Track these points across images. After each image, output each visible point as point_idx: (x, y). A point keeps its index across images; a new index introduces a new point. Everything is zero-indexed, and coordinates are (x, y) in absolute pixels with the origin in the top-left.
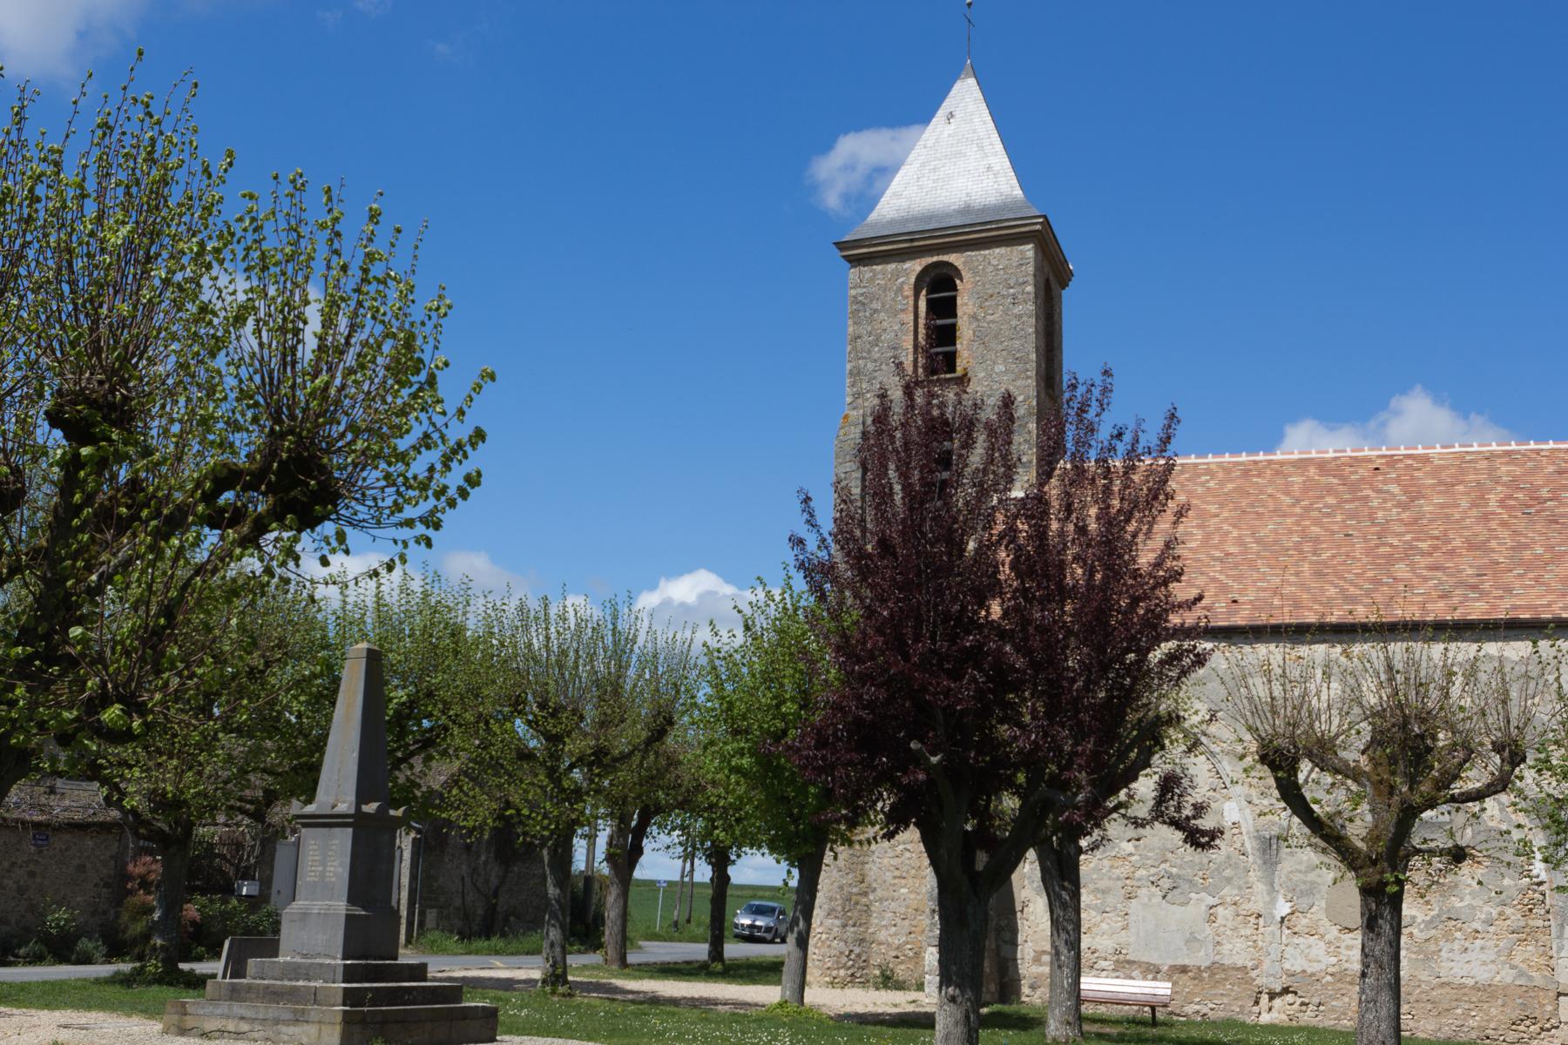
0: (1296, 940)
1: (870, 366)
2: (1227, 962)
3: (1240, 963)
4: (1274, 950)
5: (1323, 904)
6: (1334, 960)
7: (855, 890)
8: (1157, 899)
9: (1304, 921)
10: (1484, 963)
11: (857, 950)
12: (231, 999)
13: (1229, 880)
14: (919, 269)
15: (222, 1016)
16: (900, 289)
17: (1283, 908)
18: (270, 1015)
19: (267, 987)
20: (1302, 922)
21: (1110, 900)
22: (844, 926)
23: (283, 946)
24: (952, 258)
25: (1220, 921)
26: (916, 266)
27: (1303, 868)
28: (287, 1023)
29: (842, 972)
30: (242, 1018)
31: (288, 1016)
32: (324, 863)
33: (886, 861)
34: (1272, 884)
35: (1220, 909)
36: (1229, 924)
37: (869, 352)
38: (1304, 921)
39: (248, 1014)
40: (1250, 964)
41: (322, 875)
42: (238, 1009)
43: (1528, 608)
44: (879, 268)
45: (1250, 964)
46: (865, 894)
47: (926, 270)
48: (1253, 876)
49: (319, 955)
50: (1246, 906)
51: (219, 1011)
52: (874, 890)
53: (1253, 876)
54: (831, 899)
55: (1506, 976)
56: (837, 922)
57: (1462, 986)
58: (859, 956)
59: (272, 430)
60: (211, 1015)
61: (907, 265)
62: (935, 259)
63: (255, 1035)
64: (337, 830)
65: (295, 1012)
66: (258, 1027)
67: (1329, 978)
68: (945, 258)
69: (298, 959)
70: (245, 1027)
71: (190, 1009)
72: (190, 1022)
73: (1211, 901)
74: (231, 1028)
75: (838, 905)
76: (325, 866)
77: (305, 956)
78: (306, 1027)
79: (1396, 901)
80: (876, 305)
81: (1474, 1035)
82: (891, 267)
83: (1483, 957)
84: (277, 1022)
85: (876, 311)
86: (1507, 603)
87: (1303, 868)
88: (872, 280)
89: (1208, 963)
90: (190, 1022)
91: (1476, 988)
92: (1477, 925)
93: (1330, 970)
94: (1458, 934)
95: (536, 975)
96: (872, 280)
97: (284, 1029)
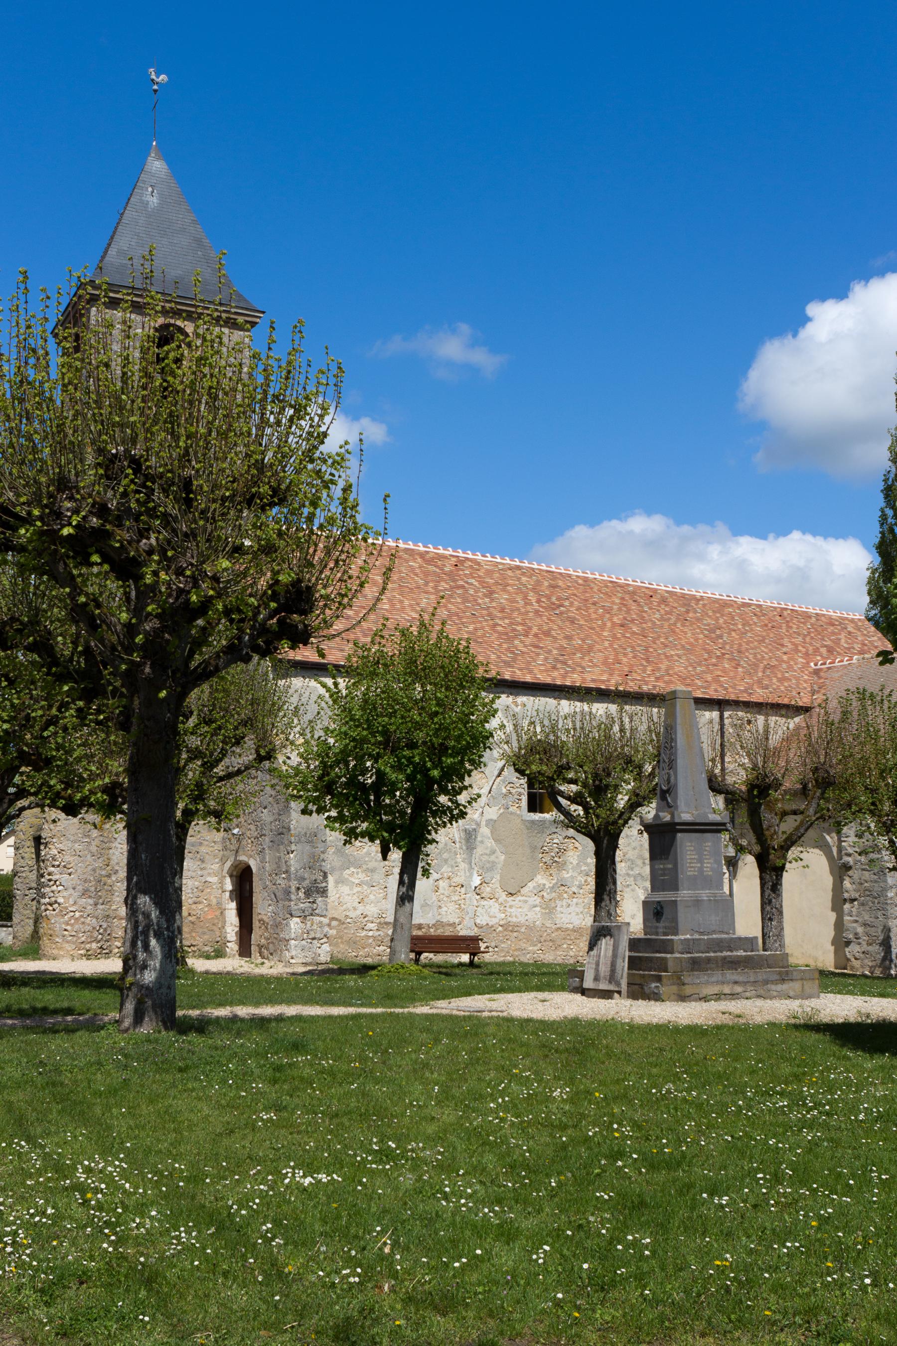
0: (483, 902)
2: (444, 920)
3: (451, 921)
4: (471, 910)
5: (498, 877)
6: (503, 916)
7: (103, 873)
9: (488, 889)
10: (577, 914)
11: (105, 925)
12: (692, 970)
13: (446, 861)
15: (717, 982)
17: (476, 881)
18: (760, 978)
19: (725, 958)
20: (486, 890)
21: (376, 877)
22: (96, 905)
23: (681, 926)
25: (441, 891)
27: (488, 852)
28: (772, 982)
29: (94, 945)
30: (736, 983)
31: (776, 977)
32: (701, 861)
34: (470, 863)
35: (441, 882)
36: (446, 893)
38: (488, 889)
39: (740, 978)
40: (457, 921)
41: (701, 870)
42: (731, 975)
43: (593, 681)
45: (457, 921)
46: (109, 876)
48: (459, 858)
49: (714, 932)
50: (455, 880)
51: (714, 979)
53: (459, 858)
54: (85, 881)
56: (91, 901)
57: (567, 929)
58: (105, 930)
60: (708, 983)
63: (748, 994)
64: (708, 835)
65: (780, 973)
66: (749, 988)
67: (500, 928)
69: (697, 936)
70: (738, 989)
72: (688, 990)
74: (727, 990)
75: (91, 886)
76: (702, 863)
77: (702, 933)
78: (791, 984)
79: (780, 870)
81: (572, 961)
83: (578, 910)
84: (766, 982)
86: (588, 677)
87: (488, 852)
89: (434, 922)
90: (688, 990)
92: (574, 889)
93: (502, 923)
94: (565, 895)
97: (773, 987)
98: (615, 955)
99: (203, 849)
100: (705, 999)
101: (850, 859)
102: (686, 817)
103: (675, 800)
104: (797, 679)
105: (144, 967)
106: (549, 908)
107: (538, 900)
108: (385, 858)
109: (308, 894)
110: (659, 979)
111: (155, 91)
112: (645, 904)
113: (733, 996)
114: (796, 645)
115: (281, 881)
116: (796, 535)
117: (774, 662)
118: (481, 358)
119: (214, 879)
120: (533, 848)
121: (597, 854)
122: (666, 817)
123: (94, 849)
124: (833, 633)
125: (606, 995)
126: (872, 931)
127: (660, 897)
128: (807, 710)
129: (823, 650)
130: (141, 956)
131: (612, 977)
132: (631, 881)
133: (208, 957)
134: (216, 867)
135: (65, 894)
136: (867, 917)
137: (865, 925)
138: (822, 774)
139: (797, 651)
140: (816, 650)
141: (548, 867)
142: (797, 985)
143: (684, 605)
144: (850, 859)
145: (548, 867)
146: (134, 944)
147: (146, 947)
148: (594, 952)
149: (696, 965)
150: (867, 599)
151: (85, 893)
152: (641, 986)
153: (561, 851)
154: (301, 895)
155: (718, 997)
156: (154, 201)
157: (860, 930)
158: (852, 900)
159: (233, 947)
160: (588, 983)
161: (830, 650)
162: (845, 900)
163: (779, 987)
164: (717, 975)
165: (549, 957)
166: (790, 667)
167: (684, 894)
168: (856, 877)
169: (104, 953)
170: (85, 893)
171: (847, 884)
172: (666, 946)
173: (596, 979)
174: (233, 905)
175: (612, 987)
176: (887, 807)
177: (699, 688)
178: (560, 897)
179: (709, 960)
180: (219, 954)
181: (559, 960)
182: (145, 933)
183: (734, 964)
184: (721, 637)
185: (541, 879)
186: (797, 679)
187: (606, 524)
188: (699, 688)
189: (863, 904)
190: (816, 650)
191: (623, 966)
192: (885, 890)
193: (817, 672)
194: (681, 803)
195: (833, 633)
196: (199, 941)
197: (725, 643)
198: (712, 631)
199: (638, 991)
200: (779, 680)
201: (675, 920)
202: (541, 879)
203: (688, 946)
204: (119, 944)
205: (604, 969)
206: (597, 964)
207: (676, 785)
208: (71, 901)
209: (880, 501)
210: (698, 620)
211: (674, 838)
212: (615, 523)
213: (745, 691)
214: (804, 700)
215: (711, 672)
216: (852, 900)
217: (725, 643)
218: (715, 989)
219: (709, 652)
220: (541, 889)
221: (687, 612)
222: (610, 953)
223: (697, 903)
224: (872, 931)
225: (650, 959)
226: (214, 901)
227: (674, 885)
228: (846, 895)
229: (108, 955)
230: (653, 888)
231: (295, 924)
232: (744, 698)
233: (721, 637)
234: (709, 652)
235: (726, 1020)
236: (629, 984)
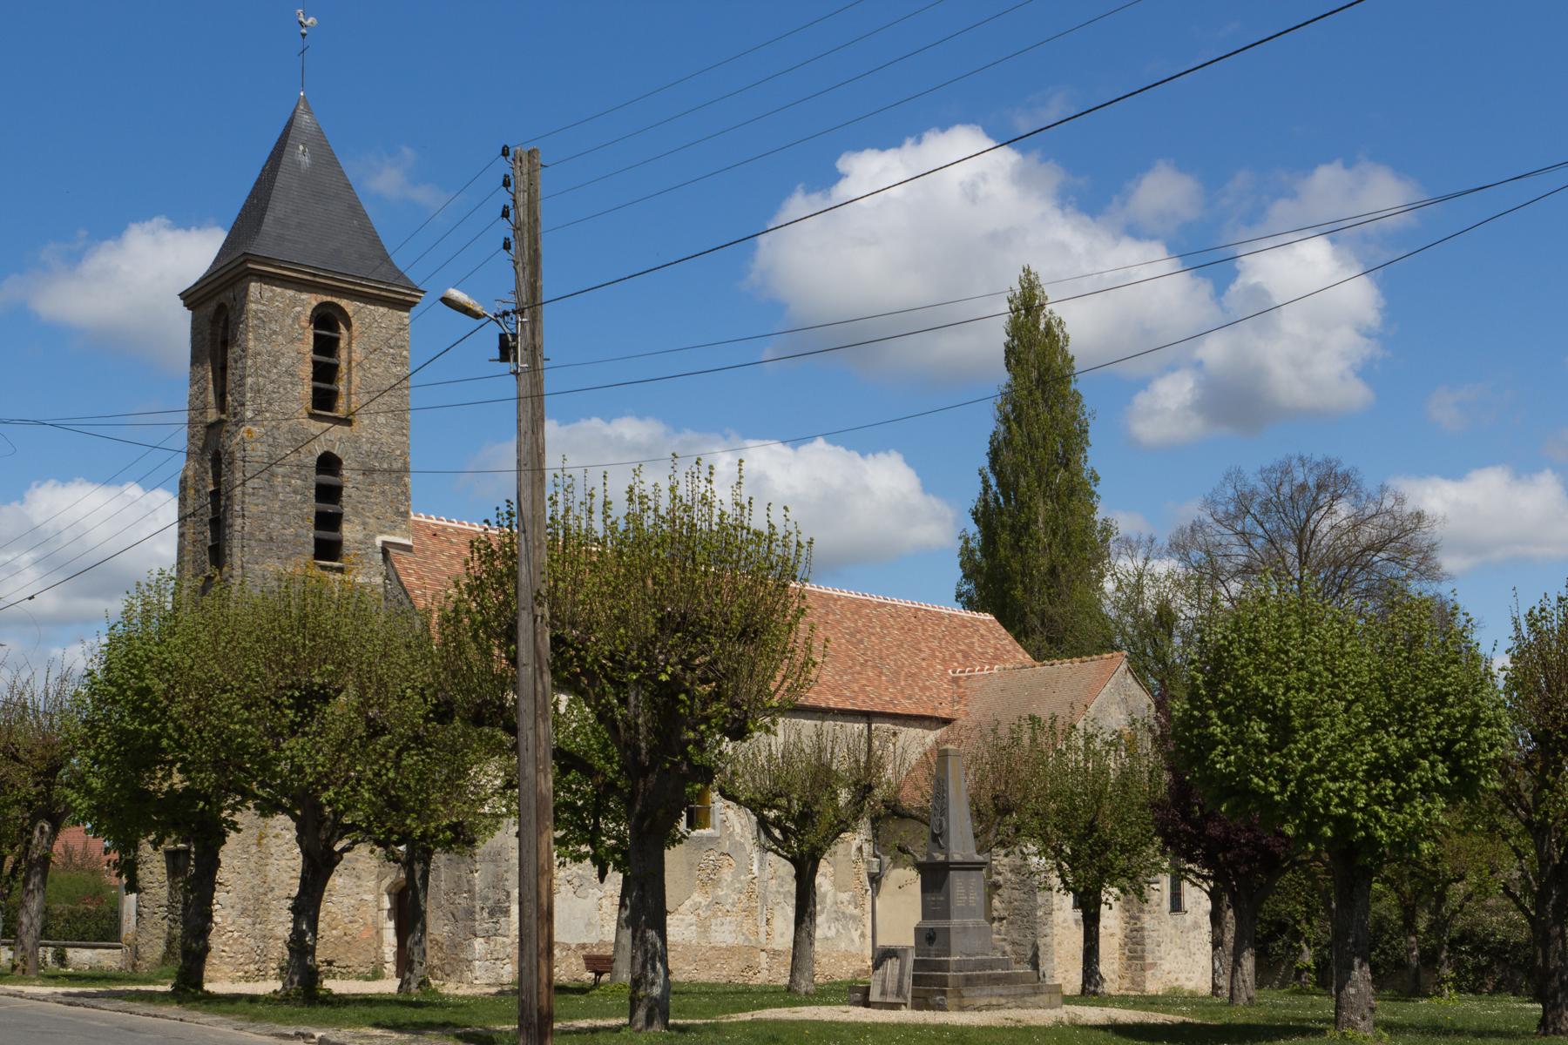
1: (270, 387)
8: (571, 894)
14: (315, 303)
16: (297, 318)
24: (343, 303)
26: (311, 300)
28: (1029, 995)
29: (252, 967)
33: (283, 863)
37: (269, 372)
39: (1005, 992)
41: (967, 902)
42: (997, 990)
44: (279, 290)
47: (322, 305)
52: (272, 890)
55: (740, 940)
56: (249, 921)
59: (1448, 694)
61: (304, 296)
62: (329, 299)
68: (335, 300)
70: (1003, 1001)
71: (965, 993)
72: (966, 1002)
73: (600, 894)
74: (994, 1002)
80: (274, 326)
82: (290, 293)
84: (1023, 995)
85: (275, 332)
88: (271, 299)
90: (966, 1002)
91: (727, 949)
95: (168, 988)
96: (271, 299)
98: (902, 974)
99: (359, 866)
100: (979, 1009)
101: (1000, 878)
102: (957, 857)
103: (947, 842)
104: (937, 687)
105: (653, 983)
106: (704, 927)
107: (693, 918)
108: (602, 881)
109: (492, 914)
110: (944, 993)
111: (304, 35)
112: (917, 930)
113: (999, 1007)
114: (933, 650)
115: (462, 900)
116: (820, 443)
117: (914, 670)
118: (425, 196)
119: (369, 897)
120: (691, 865)
121: (798, 877)
122: (941, 858)
123: (252, 865)
124: (967, 636)
125: (894, 1006)
126: (1020, 949)
127: (931, 924)
128: (946, 722)
129: (959, 655)
130: (651, 975)
131: (899, 992)
132: (780, 898)
133: (367, 979)
134: (372, 884)
135: (223, 913)
136: (1015, 936)
137: (1013, 943)
138: (1001, 802)
139: (934, 656)
140: (953, 656)
141: (704, 884)
142: (1045, 998)
143: (824, 606)
144: (1000, 878)
145: (704, 884)
146: (644, 967)
147: (654, 968)
148: (880, 971)
149: (969, 981)
150: (960, 573)
151: (244, 912)
152: (926, 999)
153: (717, 868)
154: (485, 915)
155: (989, 1007)
156: (305, 160)
157: (1008, 948)
158: (1001, 919)
159: (390, 968)
160: (875, 996)
161: (966, 656)
162: (994, 919)
163: (1033, 999)
164: (987, 990)
165: (703, 977)
166: (930, 675)
167: (955, 922)
168: (1006, 896)
169: (261, 975)
170: (244, 912)
171: (996, 902)
172: (944, 966)
173: (883, 993)
174: (391, 924)
175: (899, 1000)
176: (1205, 872)
177: (848, 698)
178: (715, 916)
179: (978, 977)
180: (377, 975)
181: (713, 980)
182: (653, 958)
183: (996, 980)
184: (861, 641)
185: (697, 897)
186: (937, 687)
187: (584, 424)
188: (848, 698)
189: (1011, 923)
190: (953, 656)
191: (908, 982)
192: (1034, 909)
193: (955, 680)
194: (952, 845)
195: (967, 636)
196: (354, 962)
197: (866, 649)
198: (852, 635)
199: (921, 1003)
200: (921, 689)
201: (948, 944)
202: (697, 897)
203: (961, 966)
204: (274, 965)
205: (891, 985)
206: (884, 981)
207: (948, 830)
208: (230, 921)
209: (985, 462)
210: (838, 622)
211: (946, 876)
212: (596, 422)
213: (891, 702)
214: (943, 713)
215: (856, 681)
216: (1001, 919)
217: (866, 649)
218: (984, 1001)
219: (853, 659)
220: (696, 908)
221: (827, 614)
222: (897, 971)
223: (965, 929)
224: (1020, 949)
225: (931, 977)
226: (370, 920)
227: (946, 915)
228: (995, 914)
229: (265, 977)
230: (924, 917)
231: (479, 944)
232: (890, 709)
233: (861, 641)
234: (853, 659)
235: (1009, 1024)
236: (913, 997)
